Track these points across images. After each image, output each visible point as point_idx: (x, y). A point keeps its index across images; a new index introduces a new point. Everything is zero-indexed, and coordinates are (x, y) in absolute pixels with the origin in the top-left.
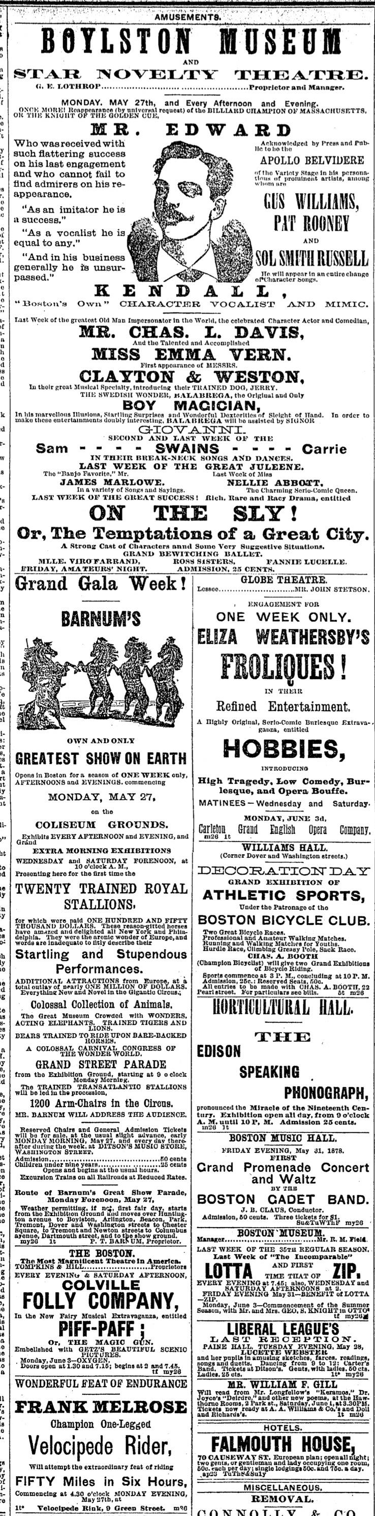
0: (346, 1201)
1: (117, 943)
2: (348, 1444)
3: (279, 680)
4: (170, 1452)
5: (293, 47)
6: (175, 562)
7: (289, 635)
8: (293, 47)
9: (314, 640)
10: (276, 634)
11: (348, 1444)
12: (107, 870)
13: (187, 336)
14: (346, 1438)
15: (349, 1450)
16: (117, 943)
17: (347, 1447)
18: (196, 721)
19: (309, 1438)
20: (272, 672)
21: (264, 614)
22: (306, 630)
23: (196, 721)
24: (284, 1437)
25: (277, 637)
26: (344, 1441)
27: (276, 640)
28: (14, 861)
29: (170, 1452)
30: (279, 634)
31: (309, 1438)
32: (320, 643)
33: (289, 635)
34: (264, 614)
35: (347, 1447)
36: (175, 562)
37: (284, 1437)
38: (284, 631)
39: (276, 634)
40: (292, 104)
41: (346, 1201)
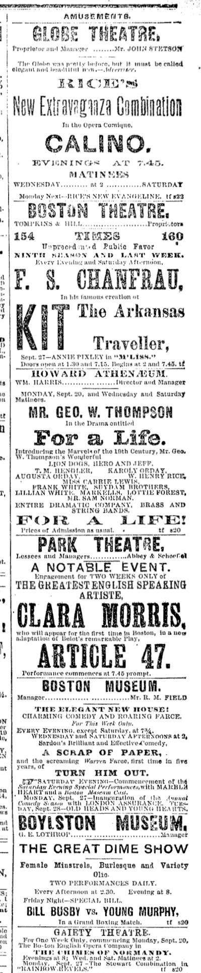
1: (115, 424)
2: (158, 544)
3: (136, 601)
4: (167, 348)
5: (124, 662)
6: (41, 743)
7: (138, 209)
8: (124, 662)
9: (119, 548)
10: (119, 542)
11: (158, 544)
13: (164, 443)
16: (115, 424)
17: (157, 547)
18: (14, 476)
21: (181, 846)
23: (14, 476)
25: (120, 545)
27: (119, 548)
28: (12, 185)
29: (167, 348)
34: (181, 846)
35: (157, 547)
36: (41, 743)
39: (124, 207)
40: (140, 247)
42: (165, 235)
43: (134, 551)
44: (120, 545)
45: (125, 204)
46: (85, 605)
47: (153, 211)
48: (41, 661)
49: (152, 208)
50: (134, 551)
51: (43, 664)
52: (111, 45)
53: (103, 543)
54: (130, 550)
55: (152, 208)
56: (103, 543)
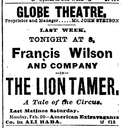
0: (85, 66)
2: (102, 12)
5: (30, 39)
7: (83, 11)
8: (30, 39)
9: (74, 14)
10: (73, 10)
11: (102, 12)
12: (49, 114)
14: (100, 8)
15: (102, 16)
17: (101, 14)
19: (68, 7)
20: (63, 39)
22: (21, 79)
24: (64, 7)
25: (74, 12)
26: (99, 10)
27: (74, 14)
30: (76, 10)
31: (68, 7)
32: (109, 93)
33: (83, 11)
35: (101, 14)
37: (64, 7)
38: (79, 8)
39: (73, 10)
41: (85, 66)
42: (56, 105)
43: (84, 17)
44: (74, 12)
45: (74, 7)
46: (56, 18)
47: (95, 12)
48: (74, 40)
49: (94, 10)
50: (84, 17)
51: (75, 41)
52: (70, 19)
53: (61, 11)
54: (82, 16)
55: (94, 10)
56: (61, 11)
